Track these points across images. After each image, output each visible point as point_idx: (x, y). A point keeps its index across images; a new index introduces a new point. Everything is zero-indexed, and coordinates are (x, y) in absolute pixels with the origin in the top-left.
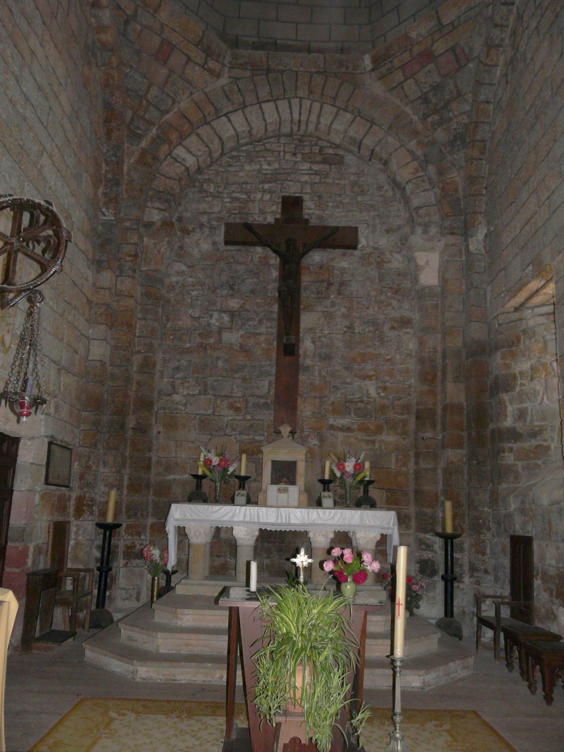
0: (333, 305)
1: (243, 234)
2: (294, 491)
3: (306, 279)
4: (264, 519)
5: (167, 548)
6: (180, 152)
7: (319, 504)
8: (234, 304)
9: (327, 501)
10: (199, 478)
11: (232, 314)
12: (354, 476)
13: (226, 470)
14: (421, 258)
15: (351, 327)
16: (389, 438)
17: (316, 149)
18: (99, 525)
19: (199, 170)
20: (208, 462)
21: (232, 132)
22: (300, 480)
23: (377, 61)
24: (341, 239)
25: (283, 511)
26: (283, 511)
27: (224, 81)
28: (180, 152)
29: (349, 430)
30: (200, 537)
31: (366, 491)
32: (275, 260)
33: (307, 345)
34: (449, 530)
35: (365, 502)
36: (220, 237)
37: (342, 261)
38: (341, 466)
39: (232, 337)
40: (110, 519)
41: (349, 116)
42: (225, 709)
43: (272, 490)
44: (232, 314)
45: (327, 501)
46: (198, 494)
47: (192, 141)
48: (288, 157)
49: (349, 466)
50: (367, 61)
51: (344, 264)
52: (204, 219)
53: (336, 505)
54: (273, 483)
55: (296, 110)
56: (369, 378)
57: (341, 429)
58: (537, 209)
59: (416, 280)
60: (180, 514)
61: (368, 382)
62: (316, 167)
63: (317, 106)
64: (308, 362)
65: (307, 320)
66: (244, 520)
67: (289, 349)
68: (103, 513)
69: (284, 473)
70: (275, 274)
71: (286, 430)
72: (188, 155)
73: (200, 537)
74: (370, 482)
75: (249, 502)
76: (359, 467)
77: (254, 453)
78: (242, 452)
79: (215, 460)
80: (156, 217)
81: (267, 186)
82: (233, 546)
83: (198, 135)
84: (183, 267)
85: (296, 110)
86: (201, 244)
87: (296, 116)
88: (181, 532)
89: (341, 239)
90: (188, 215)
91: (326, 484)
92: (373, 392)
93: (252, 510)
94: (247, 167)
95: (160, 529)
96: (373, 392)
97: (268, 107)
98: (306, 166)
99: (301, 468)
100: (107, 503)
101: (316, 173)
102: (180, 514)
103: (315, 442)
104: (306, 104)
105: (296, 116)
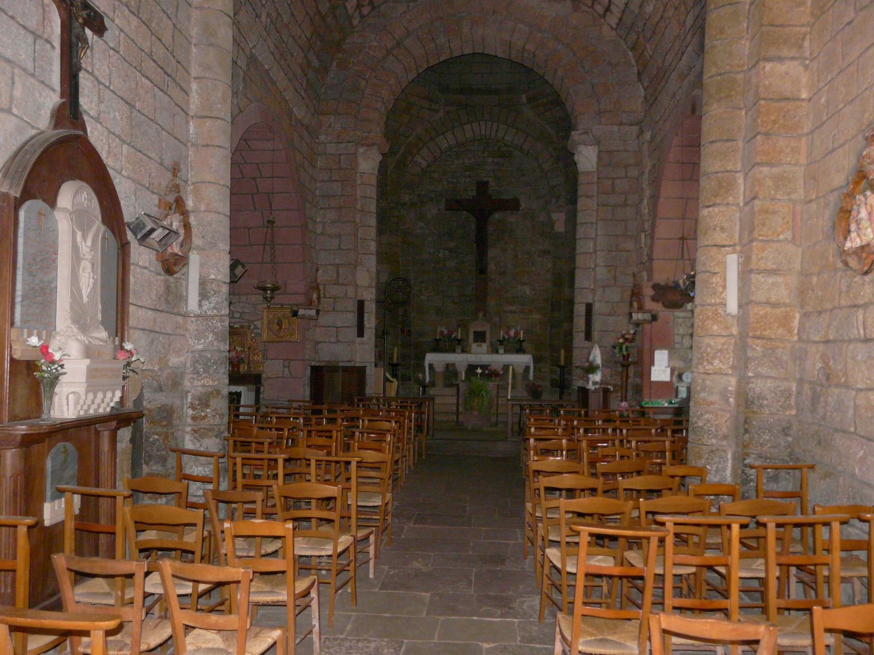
0: (506, 243)
1: (455, 205)
2: (484, 346)
3: (491, 229)
4: (62, 412)
5: (425, 373)
6: (418, 158)
7: (497, 352)
8: (452, 245)
9: (501, 351)
10: (438, 341)
11: (450, 250)
12: (514, 338)
13: (451, 336)
14: (554, 216)
15: (516, 256)
16: (536, 316)
17: (496, 148)
18: (390, 364)
19: (428, 166)
20: (442, 332)
21: (446, 145)
22: (488, 341)
23: (530, 100)
24: (512, 205)
25: (480, 355)
26: (480, 355)
27: (441, 113)
28: (418, 158)
29: (515, 312)
30: (439, 368)
31: (521, 346)
32: (472, 219)
33: (492, 267)
34: (562, 363)
35: (520, 350)
36: (442, 206)
37: (512, 218)
38: (507, 333)
39: (452, 264)
40: (395, 361)
41: (514, 131)
42: (437, 61)
43: (474, 346)
44: (450, 250)
45: (501, 351)
46: (436, 349)
47: (425, 151)
48: (479, 154)
49: (512, 333)
50: (524, 99)
51: (512, 220)
52: (433, 195)
53: (506, 351)
54: (475, 341)
55: (483, 128)
56: (525, 284)
57: (512, 312)
58: (314, 502)
59: (552, 227)
60: (430, 358)
61: (526, 287)
62: (495, 160)
63: (495, 124)
64: (493, 277)
65: (492, 253)
66: (459, 359)
67: (482, 270)
68: (391, 358)
69: (480, 337)
70: (474, 227)
71: (481, 315)
72: (422, 160)
73: (439, 368)
74: (523, 341)
75: (463, 351)
76: (517, 334)
77: (464, 326)
78: (459, 326)
79: (446, 332)
80: (407, 198)
81: (468, 173)
82: (456, 374)
83: (428, 148)
84: (422, 224)
85: (483, 128)
86: (432, 211)
87: (483, 132)
88: (431, 366)
89: (512, 205)
90: (423, 193)
91: (501, 342)
92: (528, 292)
93: (464, 355)
94: (456, 162)
95: (420, 367)
96: (528, 292)
97: (467, 127)
98: (490, 160)
99: (488, 335)
100: (393, 354)
101: (497, 164)
102: (430, 358)
103: (497, 319)
104: (489, 124)
105: (483, 132)
